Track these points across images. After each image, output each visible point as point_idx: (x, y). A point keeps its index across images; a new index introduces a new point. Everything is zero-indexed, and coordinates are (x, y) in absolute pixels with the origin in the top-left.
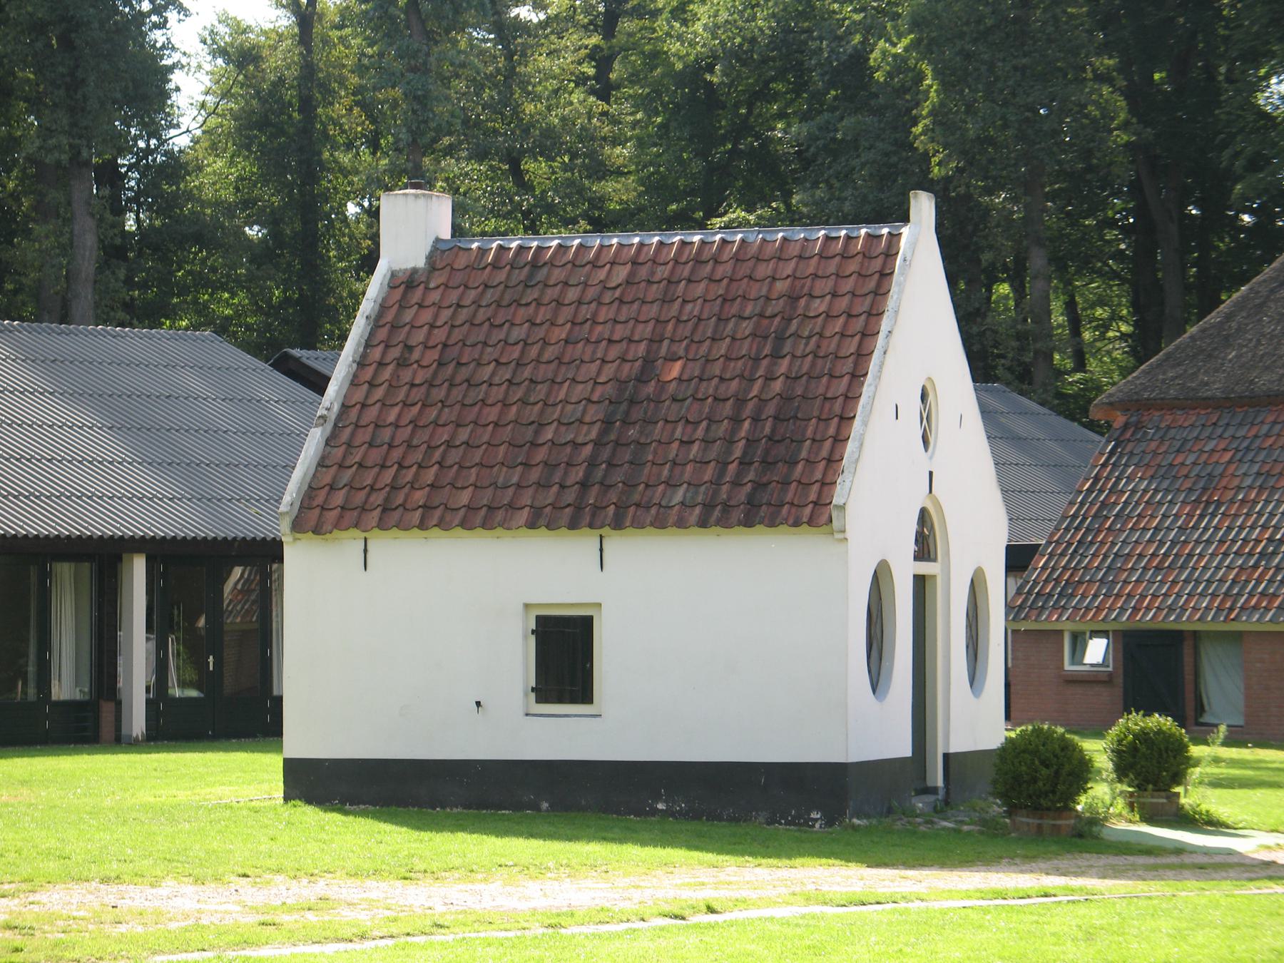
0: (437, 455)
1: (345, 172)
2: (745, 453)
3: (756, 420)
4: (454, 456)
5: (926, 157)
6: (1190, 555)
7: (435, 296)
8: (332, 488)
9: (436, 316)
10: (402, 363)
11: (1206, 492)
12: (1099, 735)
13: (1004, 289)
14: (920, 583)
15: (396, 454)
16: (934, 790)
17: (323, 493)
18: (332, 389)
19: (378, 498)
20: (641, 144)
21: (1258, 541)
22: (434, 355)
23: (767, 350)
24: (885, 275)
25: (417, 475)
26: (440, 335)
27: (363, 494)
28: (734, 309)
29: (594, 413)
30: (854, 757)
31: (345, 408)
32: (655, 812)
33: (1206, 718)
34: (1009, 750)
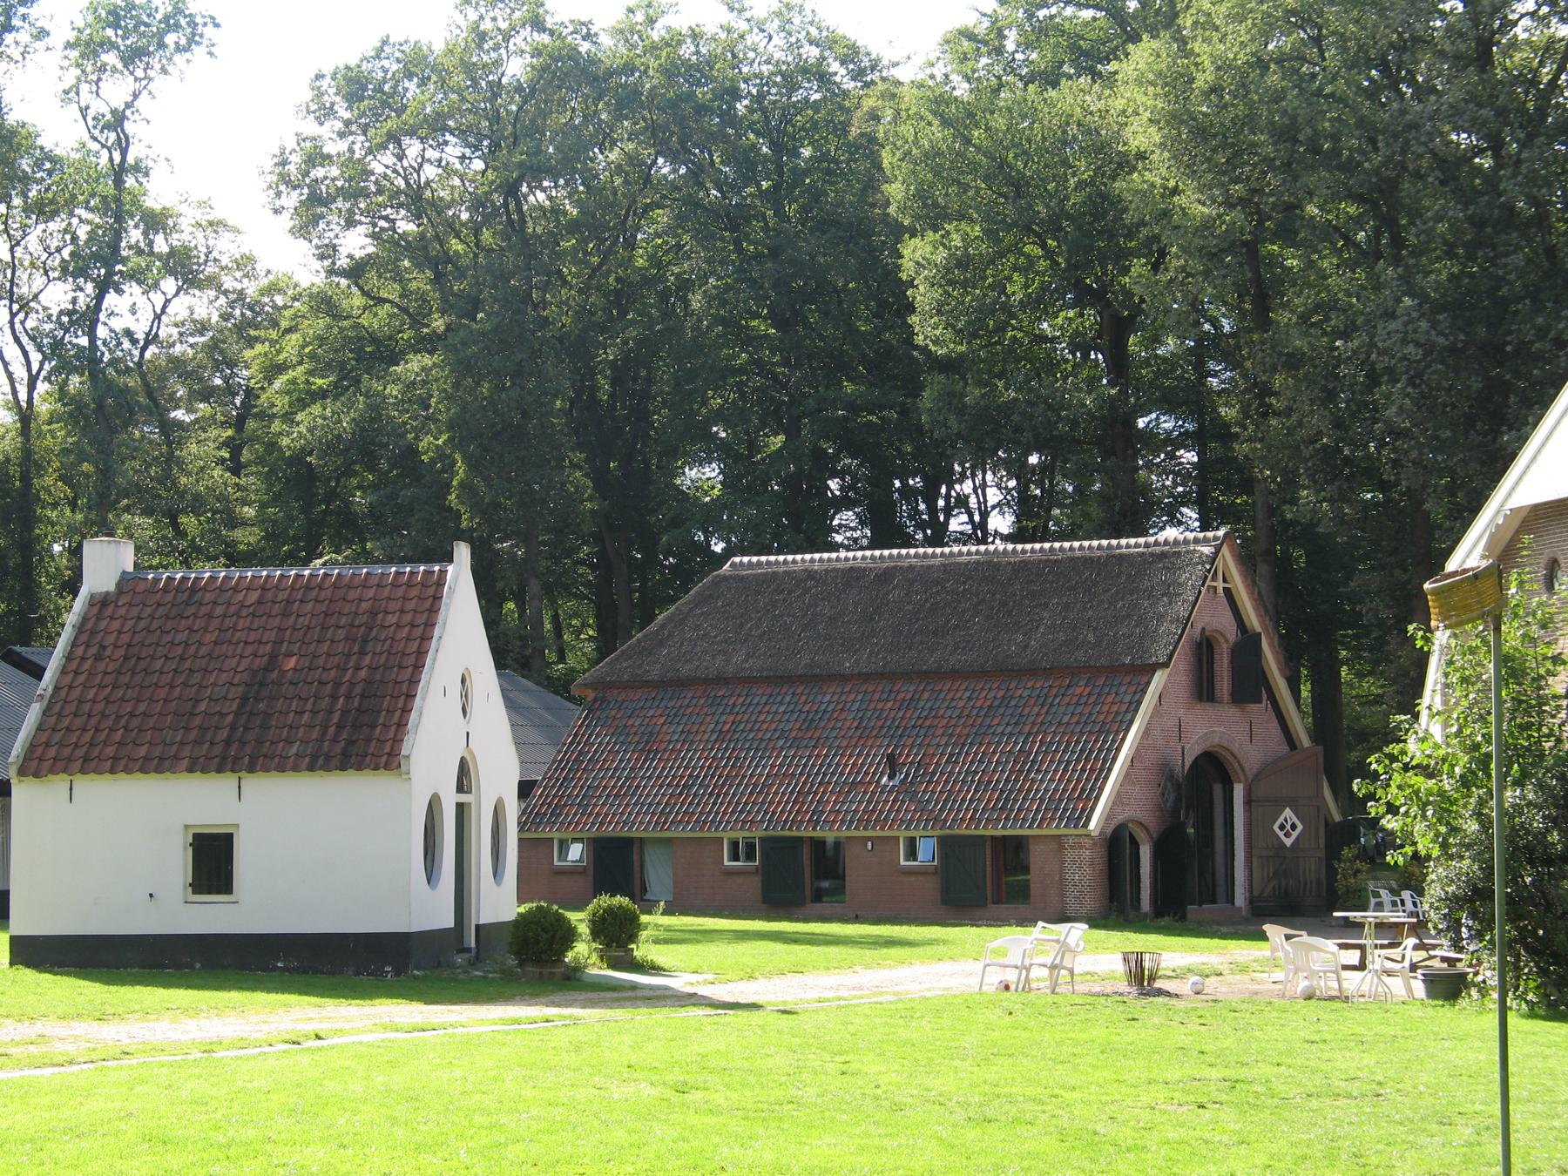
0: (123, 721)
1: (53, 524)
2: (340, 720)
3: (348, 697)
4: (135, 722)
6: (638, 787)
7: (122, 611)
8: (47, 745)
9: (123, 626)
10: (98, 658)
11: (649, 747)
13: (511, 605)
14: (461, 808)
15: (93, 721)
16: (468, 950)
17: (40, 749)
18: (47, 676)
19: (80, 752)
20: (263, 506)
21: (682, 777)
22: (121, 652)
24: (437, 598)
26: (125, 638)
27: (69, 750)
30: (415, 927)
31: (57, 689)
32: (276, 968)
33: (648, 896)
34: (522, 921)
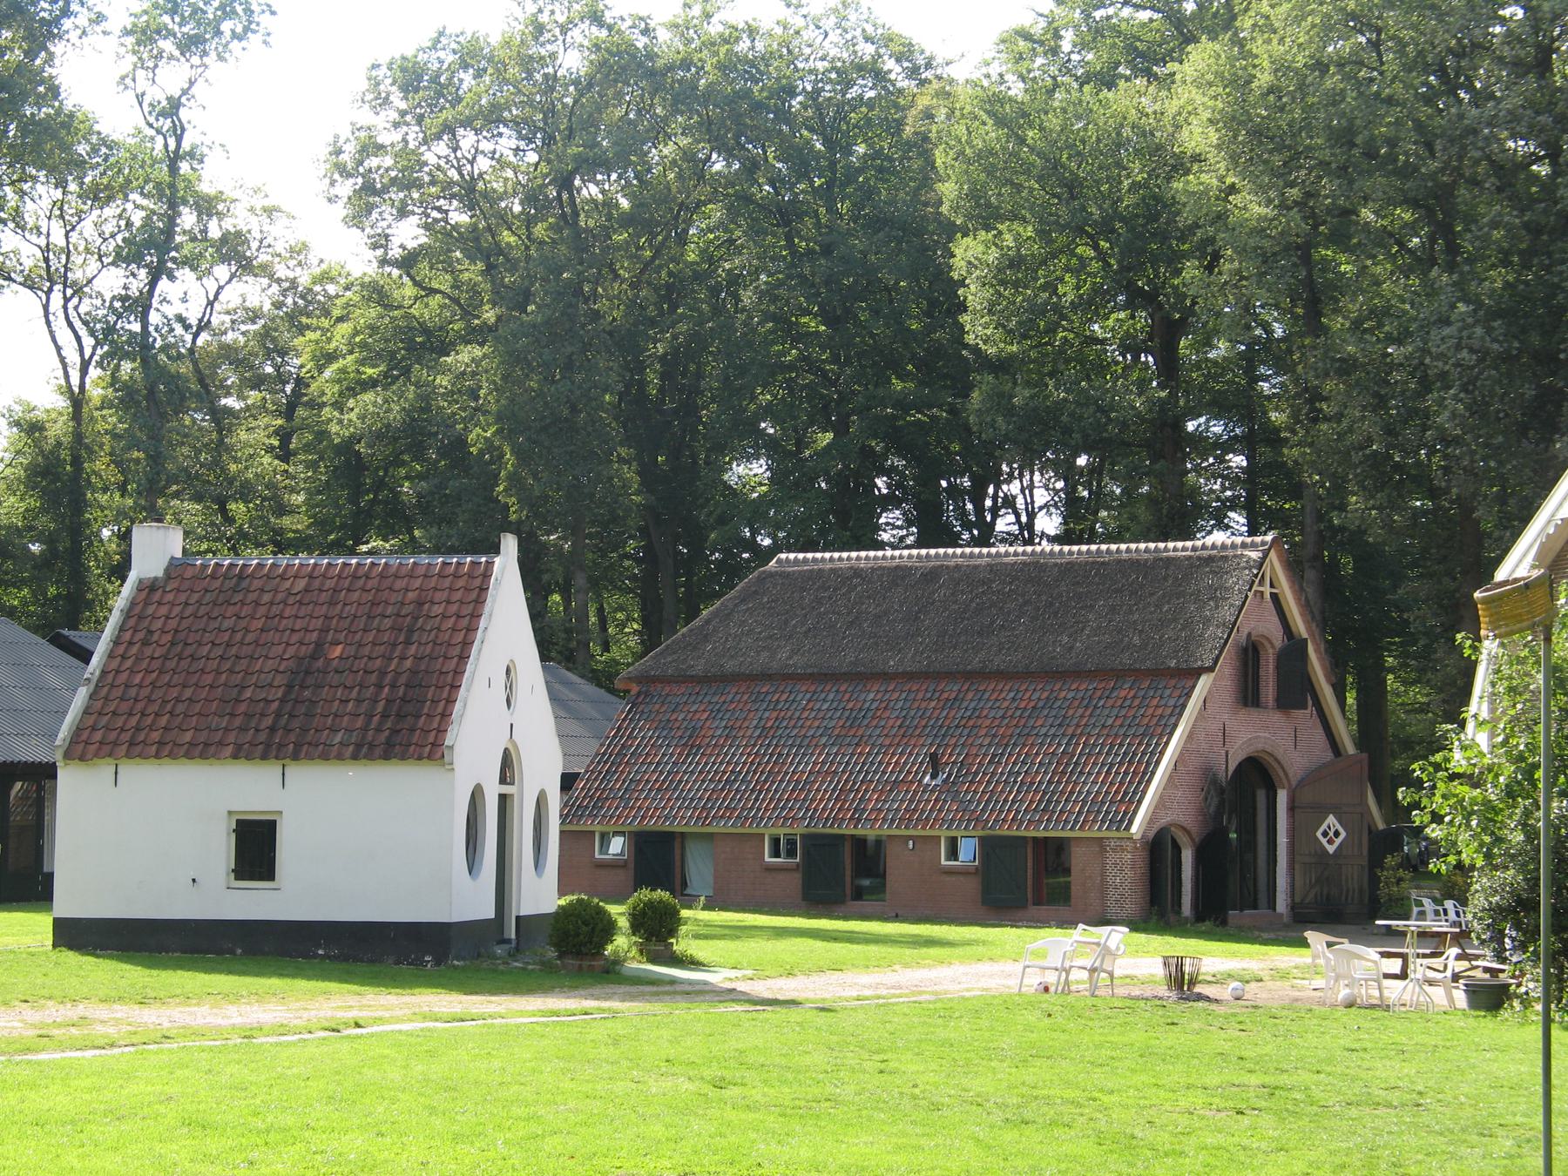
0: (169, 707)
1: (102, 509)
2: (385, 709)
3: (393, 686)
4: (181, 708)
5: (506, 507)
6: (680, 781)
8: (94, 729)
9: (170, 611)
10: (145, 643)
12: (619, 901)
13: (556, 597)
14: (503, 798)
15: (140, 706)
16: (509, 941)
18: (95, 660)
19: (126, 736)
21: (724, 772)
22: (169, 637)
23: (401, 639)
24: (483, 589)
25: (154, 721)
26: (173, 624)
28: (380, 610)
29: (280, 680)
31: (104, 673)
32: (316, 956)
33: (688, 891)
34: (563, 913)
